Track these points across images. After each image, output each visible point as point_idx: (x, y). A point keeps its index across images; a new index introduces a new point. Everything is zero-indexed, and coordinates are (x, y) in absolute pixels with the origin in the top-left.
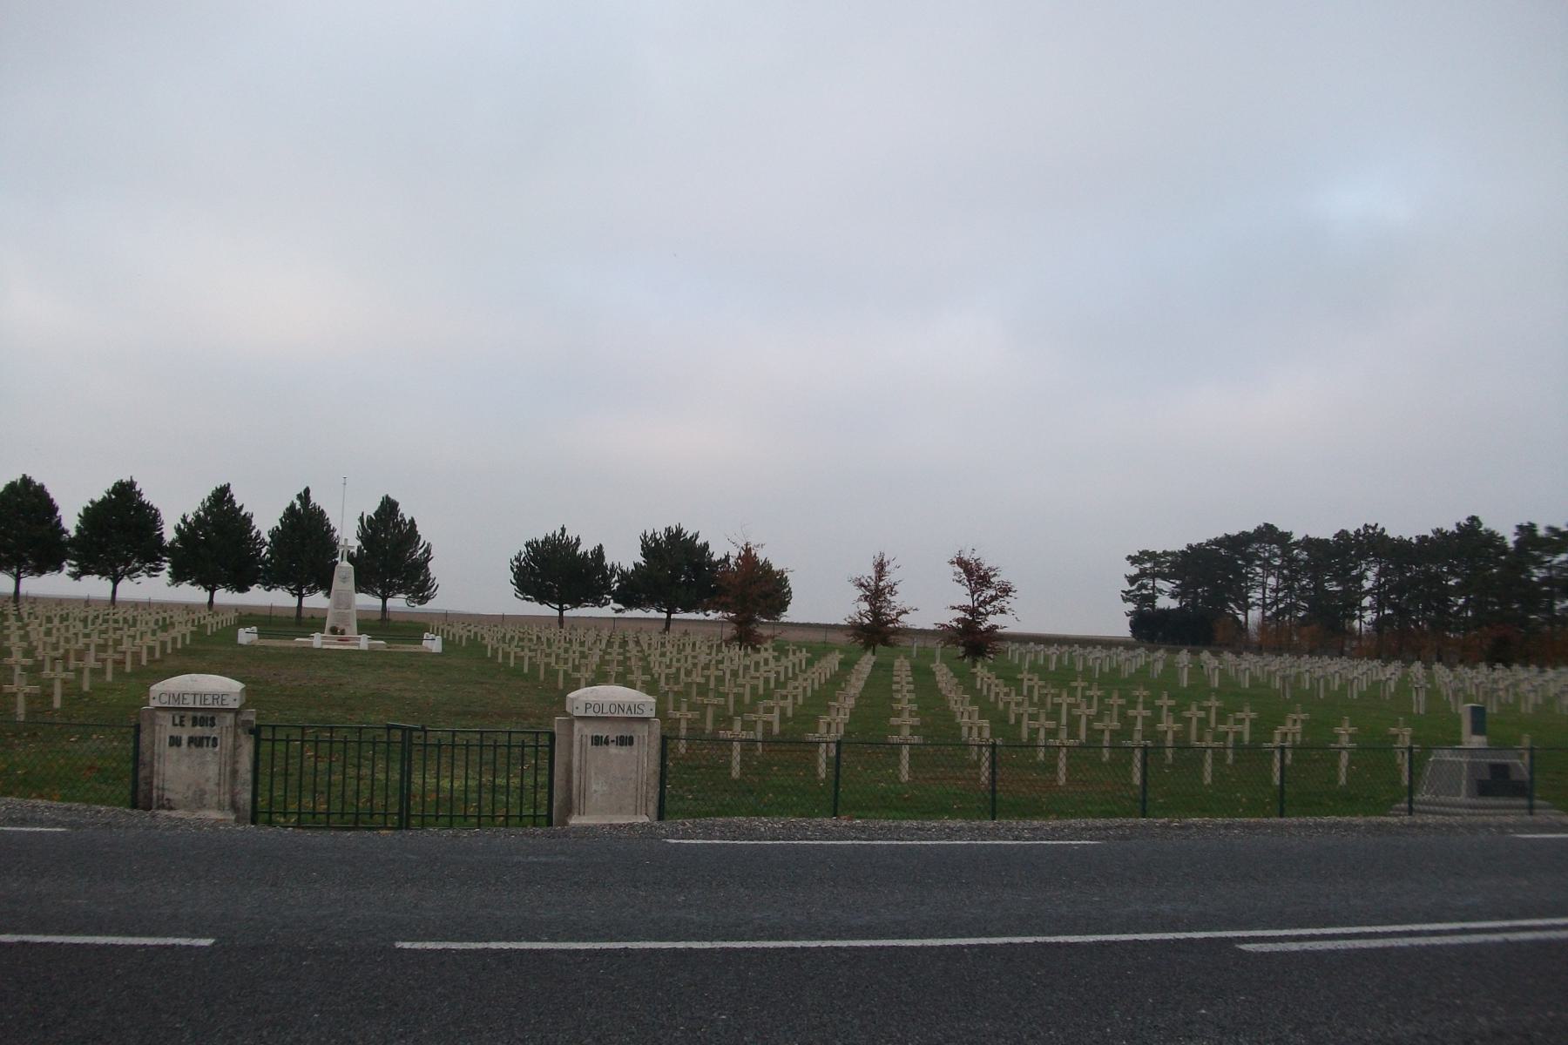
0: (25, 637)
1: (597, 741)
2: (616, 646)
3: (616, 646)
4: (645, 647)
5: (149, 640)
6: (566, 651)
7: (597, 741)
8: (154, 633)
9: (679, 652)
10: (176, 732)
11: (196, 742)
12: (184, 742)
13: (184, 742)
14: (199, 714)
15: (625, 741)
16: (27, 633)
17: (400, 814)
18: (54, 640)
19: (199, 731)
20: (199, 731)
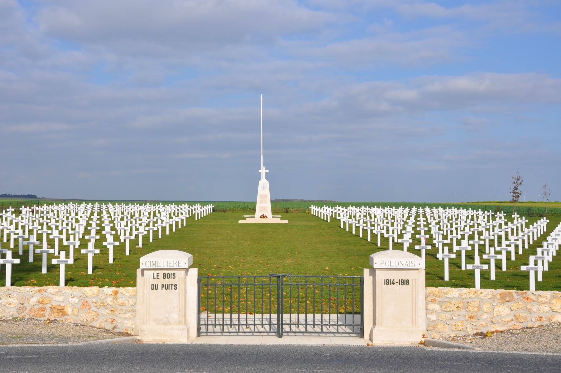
0: (113, 228)
1: (388, 282)
2: (96, 214)
3: (96, 214)
4: (112, 214)
5: (166, 224)
6: (67, 218)
7: (388, 282)
8: (506, 224)
9: (132, 217)
10: (155, 282)
11: (166, 287)
12: (160, 287)
13: (160, 287)
14: (167, 272)
15: (405, 282)
16: (114, 225)
17: (278, 324)
18: (449, 241)
19: (167, 281)
20: (167, 281)
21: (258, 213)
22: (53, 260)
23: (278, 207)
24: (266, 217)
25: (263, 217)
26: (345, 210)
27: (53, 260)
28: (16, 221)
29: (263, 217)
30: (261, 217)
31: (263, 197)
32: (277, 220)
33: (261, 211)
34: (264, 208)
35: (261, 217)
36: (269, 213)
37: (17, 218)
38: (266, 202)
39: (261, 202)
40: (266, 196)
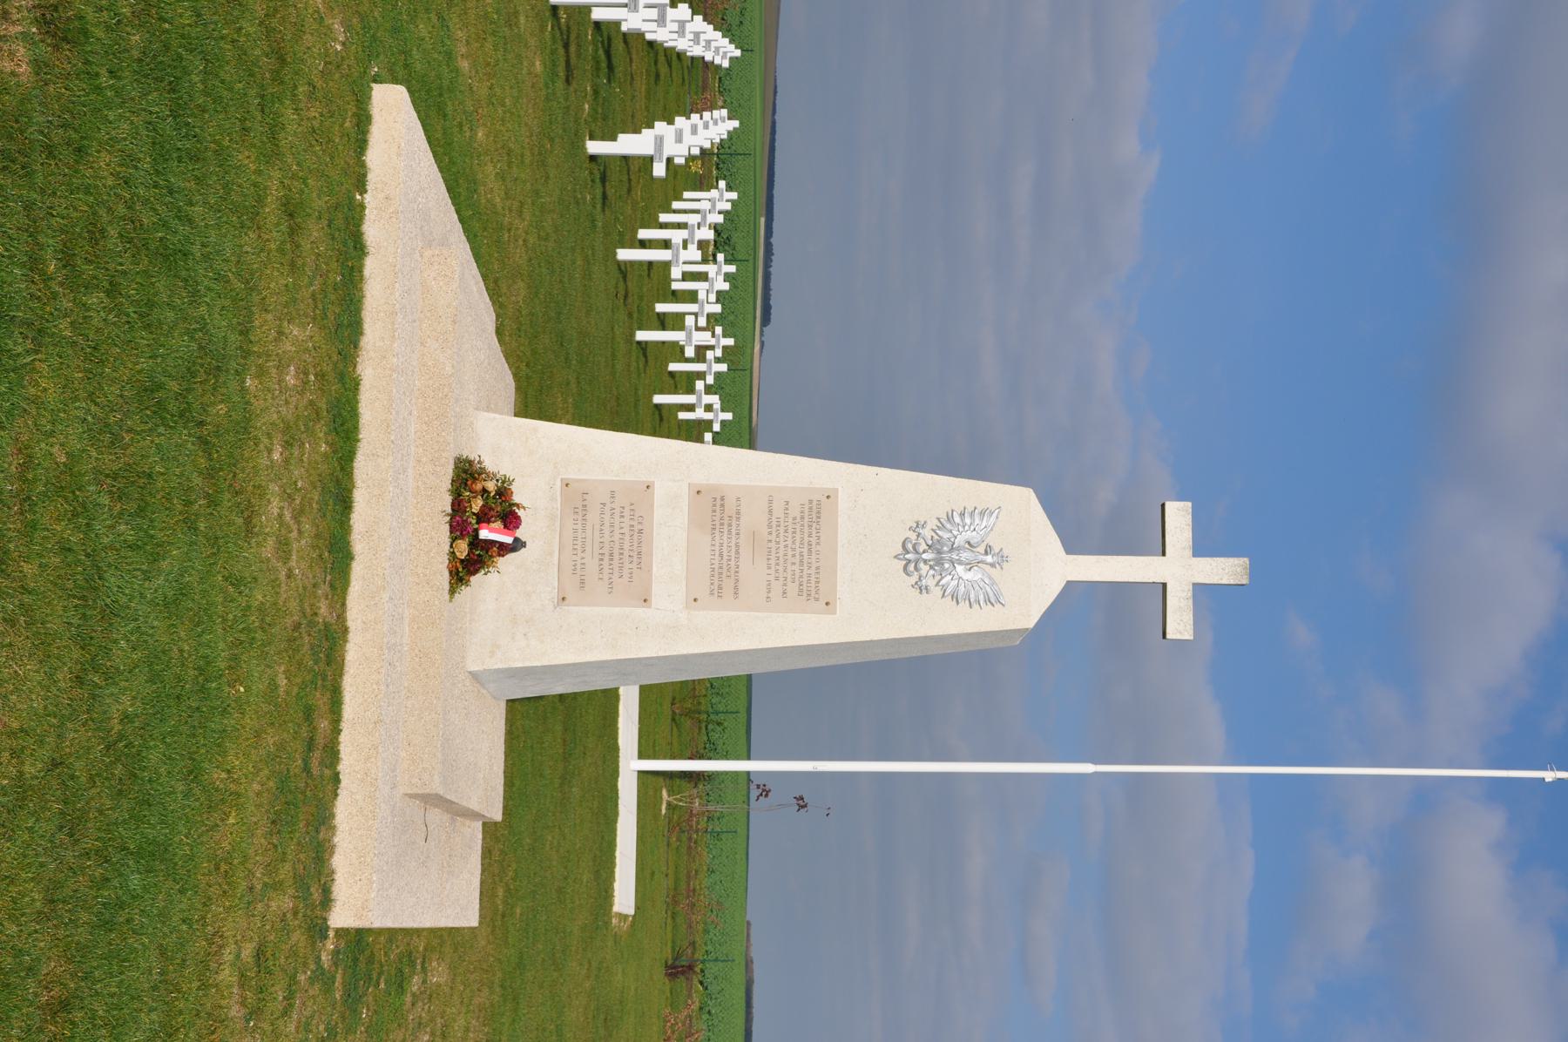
21: (546, 460)
22: (357, 903)
23: (632, 793)
24: (471, 561)
25: (480, 521)
26: (308, 36)
27: (357, 903)
28: (702, 296)
29: (480, 521)
30: (467, 475)
31: (801, 553)
32: (402, 857)
33: (576, 498)
34: (613, 548)
35: (467, 475)
36: (534, 624)
37: (721, 278)
38: (721, 583)
39: (715, 510)
40: (813, 590)
